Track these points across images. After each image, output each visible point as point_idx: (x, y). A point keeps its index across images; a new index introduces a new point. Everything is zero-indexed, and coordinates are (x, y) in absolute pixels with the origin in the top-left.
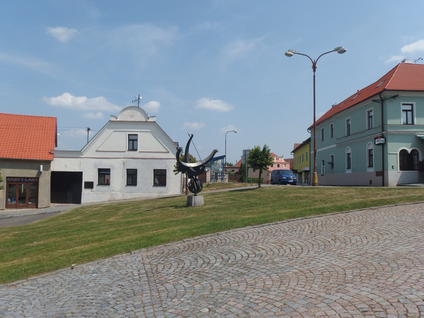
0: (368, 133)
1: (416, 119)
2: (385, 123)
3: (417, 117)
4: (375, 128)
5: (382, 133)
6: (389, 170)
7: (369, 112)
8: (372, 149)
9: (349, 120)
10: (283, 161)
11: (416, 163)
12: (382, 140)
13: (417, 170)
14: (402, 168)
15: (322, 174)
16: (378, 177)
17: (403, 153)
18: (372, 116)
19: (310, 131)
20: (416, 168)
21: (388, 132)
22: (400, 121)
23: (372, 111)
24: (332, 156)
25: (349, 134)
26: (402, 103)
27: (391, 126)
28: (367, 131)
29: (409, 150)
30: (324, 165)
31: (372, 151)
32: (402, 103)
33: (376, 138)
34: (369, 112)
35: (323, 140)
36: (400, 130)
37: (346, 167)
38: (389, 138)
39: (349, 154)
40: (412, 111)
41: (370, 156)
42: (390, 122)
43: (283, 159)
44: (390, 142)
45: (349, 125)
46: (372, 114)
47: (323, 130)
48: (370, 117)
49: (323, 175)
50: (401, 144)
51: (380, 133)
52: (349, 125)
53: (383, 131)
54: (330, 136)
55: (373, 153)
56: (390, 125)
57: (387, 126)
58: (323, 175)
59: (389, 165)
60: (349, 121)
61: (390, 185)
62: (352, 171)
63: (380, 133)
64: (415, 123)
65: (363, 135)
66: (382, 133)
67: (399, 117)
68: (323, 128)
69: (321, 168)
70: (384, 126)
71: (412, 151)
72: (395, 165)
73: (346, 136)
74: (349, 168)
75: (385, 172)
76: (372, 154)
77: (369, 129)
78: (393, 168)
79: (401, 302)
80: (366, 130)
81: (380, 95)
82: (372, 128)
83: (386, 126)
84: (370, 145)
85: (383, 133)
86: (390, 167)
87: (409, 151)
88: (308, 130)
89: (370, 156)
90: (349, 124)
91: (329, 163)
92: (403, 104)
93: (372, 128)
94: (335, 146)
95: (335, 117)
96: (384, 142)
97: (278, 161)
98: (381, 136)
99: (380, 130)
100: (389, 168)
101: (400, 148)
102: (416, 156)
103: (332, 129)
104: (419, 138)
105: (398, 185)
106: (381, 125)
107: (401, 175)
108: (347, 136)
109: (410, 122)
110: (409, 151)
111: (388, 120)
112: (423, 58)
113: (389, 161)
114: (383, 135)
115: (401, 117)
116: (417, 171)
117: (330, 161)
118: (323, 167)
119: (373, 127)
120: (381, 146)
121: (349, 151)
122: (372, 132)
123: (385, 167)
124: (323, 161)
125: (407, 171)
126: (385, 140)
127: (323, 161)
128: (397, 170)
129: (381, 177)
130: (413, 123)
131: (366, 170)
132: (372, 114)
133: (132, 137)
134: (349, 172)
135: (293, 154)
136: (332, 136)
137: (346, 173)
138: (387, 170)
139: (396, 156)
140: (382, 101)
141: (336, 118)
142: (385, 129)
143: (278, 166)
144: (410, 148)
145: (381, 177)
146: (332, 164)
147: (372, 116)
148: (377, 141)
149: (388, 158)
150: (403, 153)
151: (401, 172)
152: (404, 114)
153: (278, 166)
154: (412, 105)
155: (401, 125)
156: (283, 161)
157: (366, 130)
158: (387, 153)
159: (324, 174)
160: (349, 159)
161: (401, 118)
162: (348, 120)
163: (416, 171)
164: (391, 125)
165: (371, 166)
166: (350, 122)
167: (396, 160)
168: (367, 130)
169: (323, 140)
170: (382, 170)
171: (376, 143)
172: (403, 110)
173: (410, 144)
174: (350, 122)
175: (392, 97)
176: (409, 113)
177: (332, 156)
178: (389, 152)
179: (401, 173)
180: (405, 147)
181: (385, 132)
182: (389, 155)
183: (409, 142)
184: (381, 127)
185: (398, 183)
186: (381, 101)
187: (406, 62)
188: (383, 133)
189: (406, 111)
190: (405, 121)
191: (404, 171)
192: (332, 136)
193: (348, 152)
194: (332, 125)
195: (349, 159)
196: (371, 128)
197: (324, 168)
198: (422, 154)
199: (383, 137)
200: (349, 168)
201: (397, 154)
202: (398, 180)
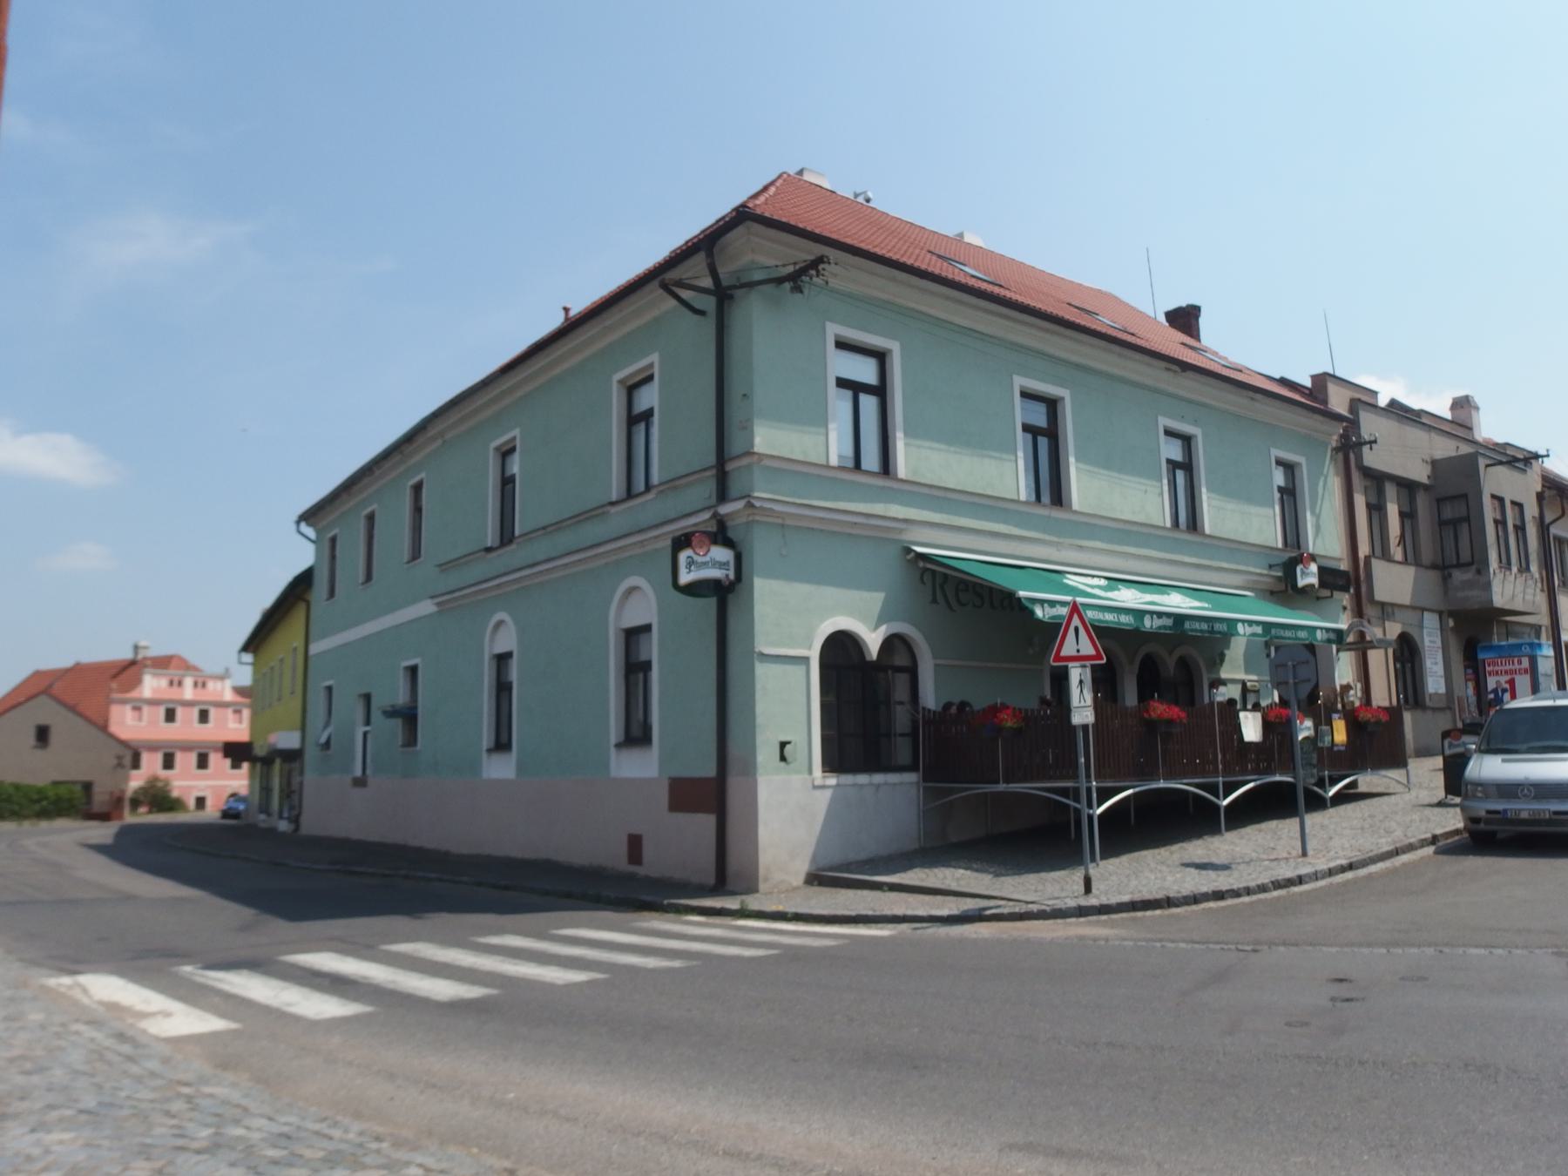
0: (620, 518)
1: (906, 445)
2: (735, 445)
3: (906, 434)
4: (672, 484)
5: (715, 515)
6: (760, 770)
7: (631, 389)
8: (647, 628)
9: (513, 450)
10: (229, 696)
11: (901, 718)
12: (711, 563)
13: (913, 768)
14: (835, 761)
15: (358, 773)
16: (682, 818)
17: (841, 647)
18: (647, 415)
19: (310, 532)
20: (903, 752)
21: (757, 504)
22: (823, 438)
23: (650, 378)
24: (413, 670)
25: (507, 536)
26: (833, 330)
27: (776, 469)
28: (613, 510)
29: (873, 635)
30: (368, 722)
31: (643, 637)
32: (833, 330)
33: (682, 542)
34: (631, 389)
35: (369, 577)
36: (826, 499)
37: (487, 739)
38: (761, 548)
39: (502, 659)
40: (880, 391)
41: (635, 670)
42: (768, 438)
43: (228, 684)
44: (771, 574)
45: (507, 482)
46: (648, 398)
47: (371, 518)
48: (637, 419)
49: (360, 782)
50: (830, 593)
51: (706, 515)
52: (507, 482)
53: (723, 496)
54: (406, 556)
55: (653, 649)
56: (766, 462)
57: (749, 466)
58: (360, 782)
59: (760, 739)
60: (508, 460)
61: (766, 880)
62: (521, 768)
63: (706, 515)
64: (902, 468)
65: (594, 531)
66: (715, 515)
67: (820, 419)
68: (369, 510)
69: (352, 740)
70: (729, 467)
71: (889, 643)
72: (795, 736)
73: (488, 550)
74: (502, 745)
75: (734, 784)
76: (643, 657)
77: (630, 494)
78: (783, 758)
79: (495, 546)
80: (612, 504)
81: (710, 255)
82: (648, 488)
83: (745, 461)
84: (635, 596)
85: (724, 509)
86: (766, 754)
87: (873, 640)
88: (298, 523)
89: (635, 670)
90: (508, 474)
91: (392, 713)
92: (842, 345)
93: (648, 488)
94: (427, 607)
95: (434, 439)
96: (732, 576)
97: (203, 695)
98: (713, 528)
99: (708, 488)
100: (760, 758)
101: (822, 621)
102: (902, 681)
103: (417, 510)
104: (921, 564)
105: (817, 879)
106: (711, 459)
107: (833, 801)
108: (497, 543)
109: (871, 460)
110: (873, 640)
111: (756, 421)
112: (870, 195)
113: (760, 707)
114: (721, 523)
115: (830, 417)
116: (911, 777)
117: (401, 698)
118: (365, 734)
119: (655, 478)
120: (711, 603)
121: (506, 641)
122: (648, 508)
123: (734, 750)
124: (367, 698)
125: (862, 779)
126: (738, 559)
127: (367, 698)
128: (810, 772)
129: (708, 821)
130: (887, 466)
131: (607, 766)
132: (648, 398)
133: (1449, 512)
134: (500, 769)
135: (248, 658)
136: (416, 554)
137: (485, 775)
138: (750, 769)
139: (797, 671)
140: (724, 295)
141: (439, 442)
142: (735, 487)
143: (204, 716)
144: (877, 627)
145: (708, 821)
146: (408, 716)
147: (647, 415)
148: (691, 563)
149: (758, 686)
150: (841, 647)
151: (832, 780)
152: (840, 404)
153: (204, 716)
154: (881, 357)
155: (828, 467)
156: (229, 696)
157: (612, 504)
158: (752, 656)
159: (368, 772)
160: (503, 689)
161: (832, 426)
162: (506, 453)
163: (893, 778)
164: (776, 464)
165: (636, 735)
166: (515, 467)
167: (804, 700)
168: (614, 498)
169: (369, 577)
170: (709, 770)
171: (685, 578)
172: (842, 383)
173: (875, 600)
174: (515, 467)
175: (779, 281)
176: (869, 403)
177: (413, 670)
178: (763, 646)
179: (828, 794)
180: (851, 614)
181: (740, 505)
182: (761, 669)
183: (876, 590)
184: (714, 472)
185: (814, 859)
186: (708, 303)
187: (807, 177)
188: (724, 509)
189: (854, 388)
190: (849, 451)
191: (848, 779)
192: (416, 554)
193: (500, 648)
194: (418, 488)
195: (503, 689)
196: (642, 487)
197: (369, 736)
198: (936, 665)
199: (721, 535)
200: (502, 745)
201: (805, 660)
202: (813, 840)
